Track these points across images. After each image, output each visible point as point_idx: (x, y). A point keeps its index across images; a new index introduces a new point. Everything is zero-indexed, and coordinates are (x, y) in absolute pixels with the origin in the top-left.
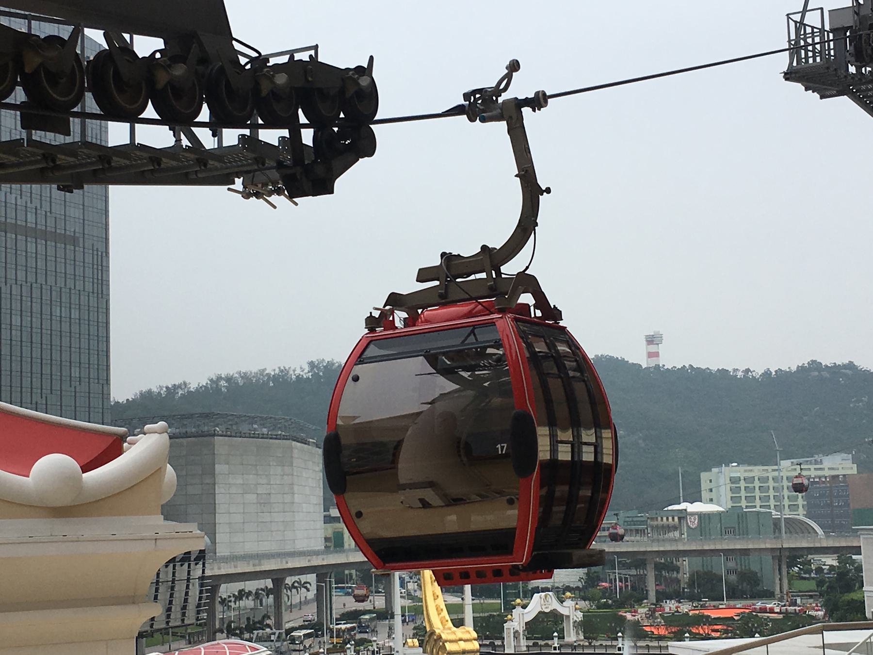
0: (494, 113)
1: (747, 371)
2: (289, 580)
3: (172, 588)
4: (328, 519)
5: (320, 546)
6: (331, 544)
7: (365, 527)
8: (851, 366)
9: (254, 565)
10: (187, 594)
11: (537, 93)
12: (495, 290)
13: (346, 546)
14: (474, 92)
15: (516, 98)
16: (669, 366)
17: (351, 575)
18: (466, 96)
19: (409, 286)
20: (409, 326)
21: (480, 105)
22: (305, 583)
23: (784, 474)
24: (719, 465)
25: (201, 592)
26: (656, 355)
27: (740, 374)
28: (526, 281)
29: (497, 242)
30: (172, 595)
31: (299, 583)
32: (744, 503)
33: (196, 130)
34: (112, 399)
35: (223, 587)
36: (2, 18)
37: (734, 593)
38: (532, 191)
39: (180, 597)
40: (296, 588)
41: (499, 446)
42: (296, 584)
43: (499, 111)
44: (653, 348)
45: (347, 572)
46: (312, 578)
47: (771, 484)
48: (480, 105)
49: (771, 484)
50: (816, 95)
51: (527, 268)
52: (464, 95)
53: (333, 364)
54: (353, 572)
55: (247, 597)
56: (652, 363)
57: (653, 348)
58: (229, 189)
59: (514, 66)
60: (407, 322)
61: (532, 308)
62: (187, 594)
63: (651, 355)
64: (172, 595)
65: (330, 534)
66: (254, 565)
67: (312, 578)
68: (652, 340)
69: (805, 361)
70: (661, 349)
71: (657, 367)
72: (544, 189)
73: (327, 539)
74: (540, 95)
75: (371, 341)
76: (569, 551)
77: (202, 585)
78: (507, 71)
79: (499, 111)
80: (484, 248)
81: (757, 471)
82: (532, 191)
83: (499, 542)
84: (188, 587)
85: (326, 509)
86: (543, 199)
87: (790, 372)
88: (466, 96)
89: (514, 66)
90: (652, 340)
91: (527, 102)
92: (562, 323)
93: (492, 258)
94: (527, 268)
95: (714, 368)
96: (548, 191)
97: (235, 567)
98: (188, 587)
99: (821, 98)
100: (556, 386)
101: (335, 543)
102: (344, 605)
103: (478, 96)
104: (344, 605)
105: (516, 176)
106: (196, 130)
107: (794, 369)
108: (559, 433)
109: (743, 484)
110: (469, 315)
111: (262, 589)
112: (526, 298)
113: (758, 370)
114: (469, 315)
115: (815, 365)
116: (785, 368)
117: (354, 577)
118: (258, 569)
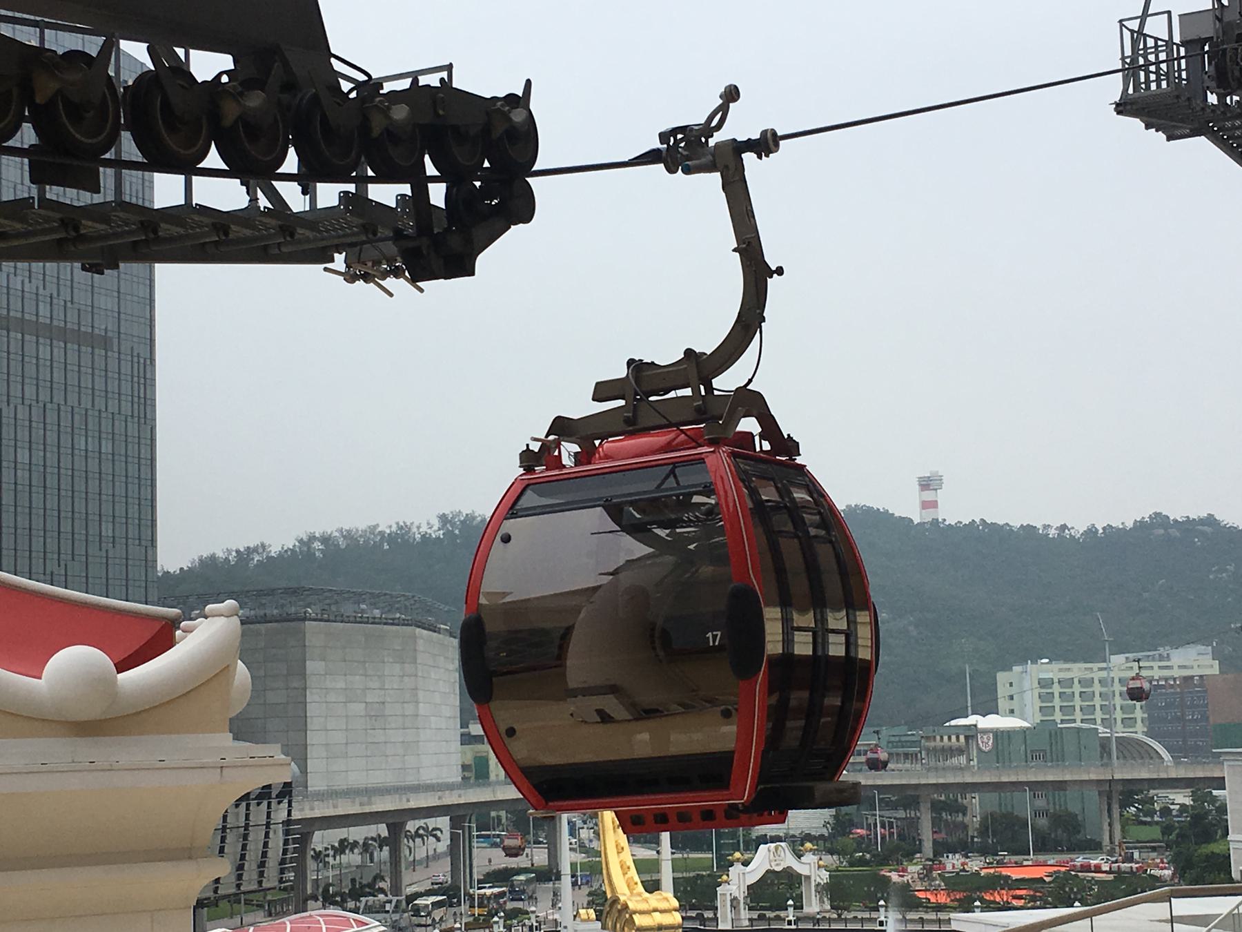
0: (703, 160)
1: (1063, 527)
2: (411, 826)
3: (245, 837)
4: (467, 739)
5: (455, 776)
6: (471, 775)
7: (519, 750)
8: (1210, 520)
9: (361, 804)
10: (266, 845)
11: (764, 133)
12: (705, 413)
13: (493, 777)
14: (674, 131)
15: (734, 140)
16: (951, 521)
17: (499, 818)
18: (663, 137)
19: (582, 406)
20: (582, 464)
21: (683, 150)
22: (434, 829)
23: (1116, 674)
24: (1023, 661)
25: (286, 842)
26: (933, 505)
27: (1052, 533)
28: (749, 401)
29: (707, 345)
30: (244, 847)
31: (426, 829)
32: (1058, 716)
33: (279, 185)
34: (159, 568)
35: (317, 835)
36: (3, 25)
38: (757, 272)
39: (257, 849)
40: (421, 836)
41: (710, 635)
42: (421, 832)
43: (710, 157)
44: (928, 496)
45: (493, 814)
46: (443, 822)
47: (1097, 688)
48: (683, 150)
49: (1097, 688)
50: (1161, 136)
51: (750, 381)
52: (661, 135)
53: (474, 518)
54: (503, 814)
55: (352, 850)
56: (928, 516)
57: (928, 496)
58: (326, 269)
59: (731, 94)
60: (579, 459)
61: (757, 439)
62: (266, 845)
63: (926, 505)
64: (244, 847)
65: (469, 759)
66: (361, 804)
67: (443, 822)
68: (927, 484)
69: (1145, 513)
70: (941, 496)
71: (935, 522)
72: (774, 268)
73: (465, 767)
74: (769, 135)
75: (528, 485)
76: (810, 784)
77: (287, 833)
78: (721, 101)
79: (710, 157)
80: (689, 353)
81: (1077, 670)
82: (757, 272)
83: (710, 771)
84: (267, 835)
85: (464, 725)
86: (773, 283)
87: (1124, 529)
88: (663, 137)
89: (731, 94)
90: (927, 484)
91: (750, 145)
92: (799, 460)
93: (700, 368)
94: (750, 381)
95: (1016, 523)
96: (780, 271)
97: (335, 807)
98: (267, 835)
99: (1169, 139)
100: (791, 549)
101: (476, 772)
102: (490, 861)
103: (680, 136)
104: (490, 861)
105: (735, 250)
106: (279, 185)
107: (1130, 524)
108: (795, 616)
109: (1056, 689)
110: (668, 448)
111: (372, 839)
112: (749, 425)
113: (1079, 527)
114: (668, 448)
115: (1159, 520)
116: (1116, 523)
117: (504, 820)
118: (367, 809)
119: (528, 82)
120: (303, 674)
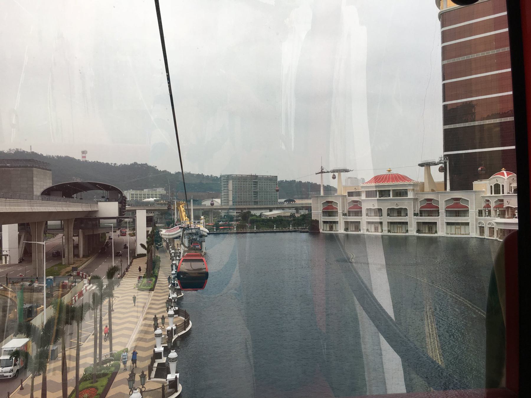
1: (115, 164)
8: (146, 164)
23: (158, 193)
26: (85, 157)
27: (113, 165)
32: (139, 199)
34: (418, 175)
37: (133, 213)
44: (84, 155)
47: (139, 196)
49: (139, 196)
56: (84, 159)
57: (84, 155)
69: (132, 162)
70: (87, 155)
71: (86, 161)
78: (475, 183)
81: (138, 192)
87: (111, 165)
90: (83, 152)
95: (105, 162)
102: (277, 191)
104: (277, 191)
107: (129, 164)
109: (135, 196)
113: (118, 164)
115: (135, 164)
116: (126, 164)
119: (421, 165)
120: (33, 181)
